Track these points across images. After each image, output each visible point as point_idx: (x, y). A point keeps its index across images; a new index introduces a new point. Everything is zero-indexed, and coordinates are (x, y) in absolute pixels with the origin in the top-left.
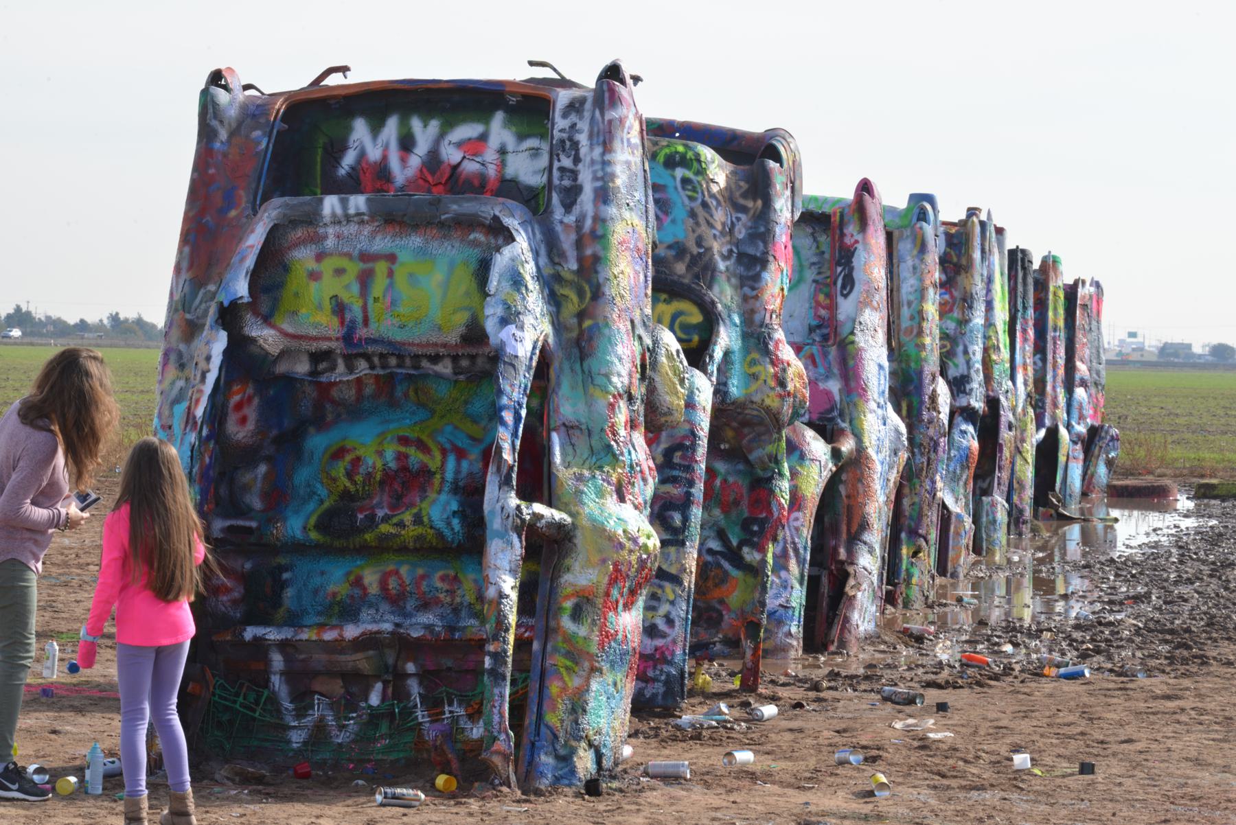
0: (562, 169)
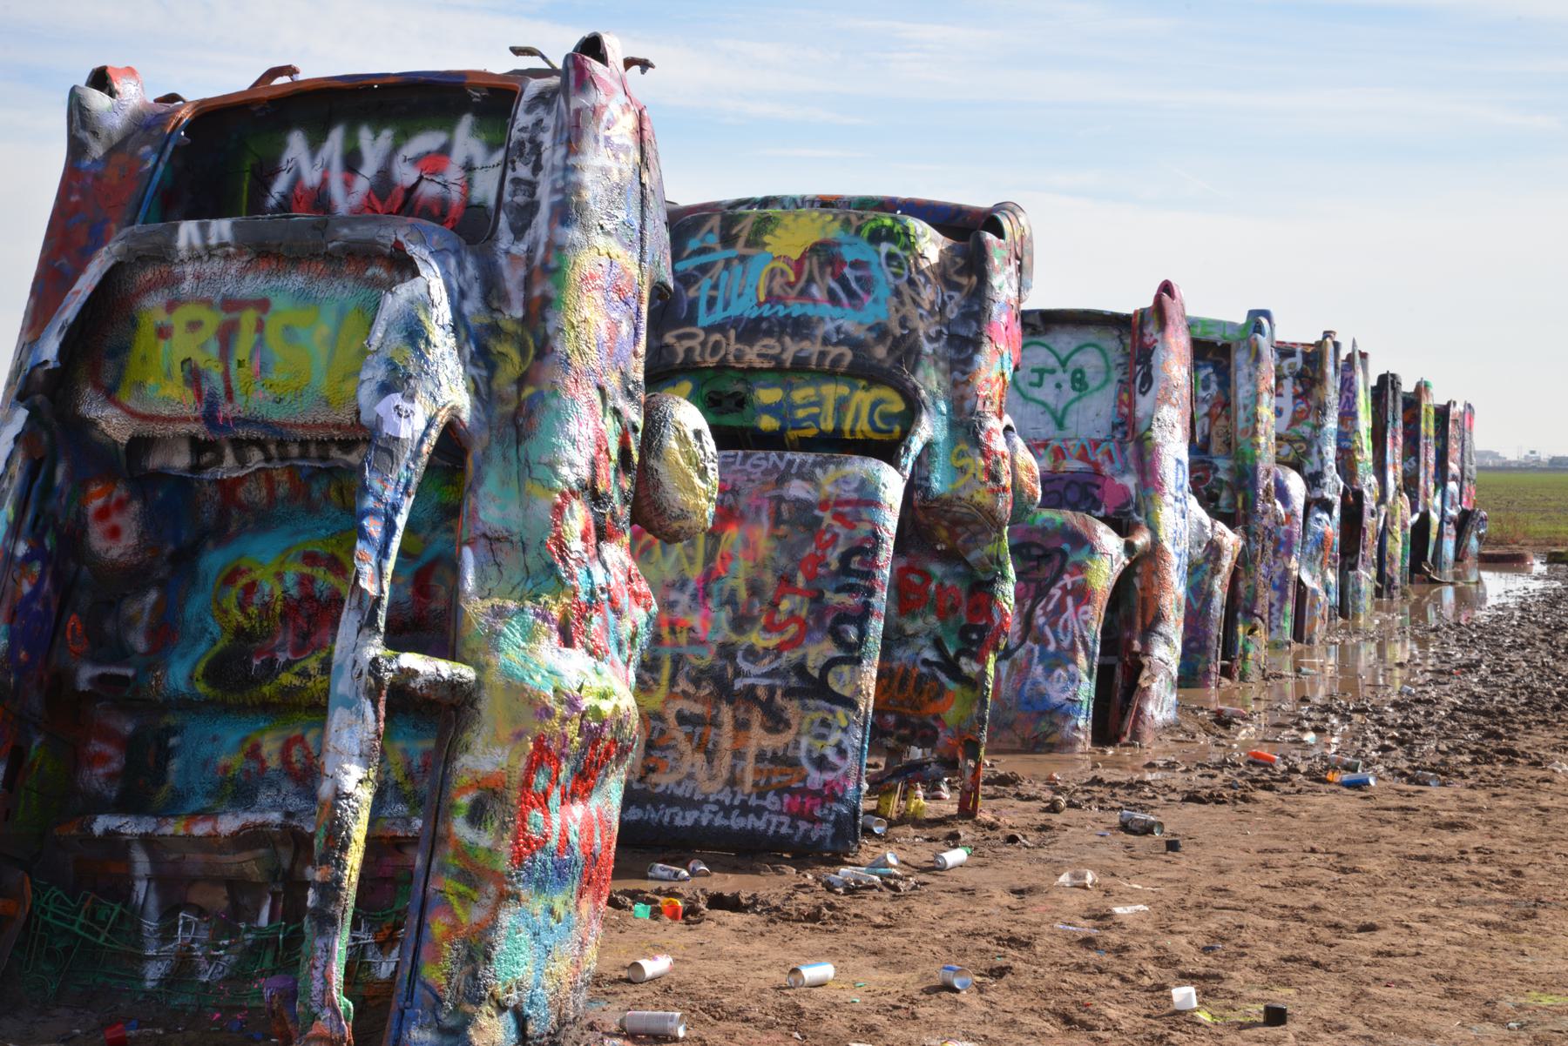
0: (517, 181)
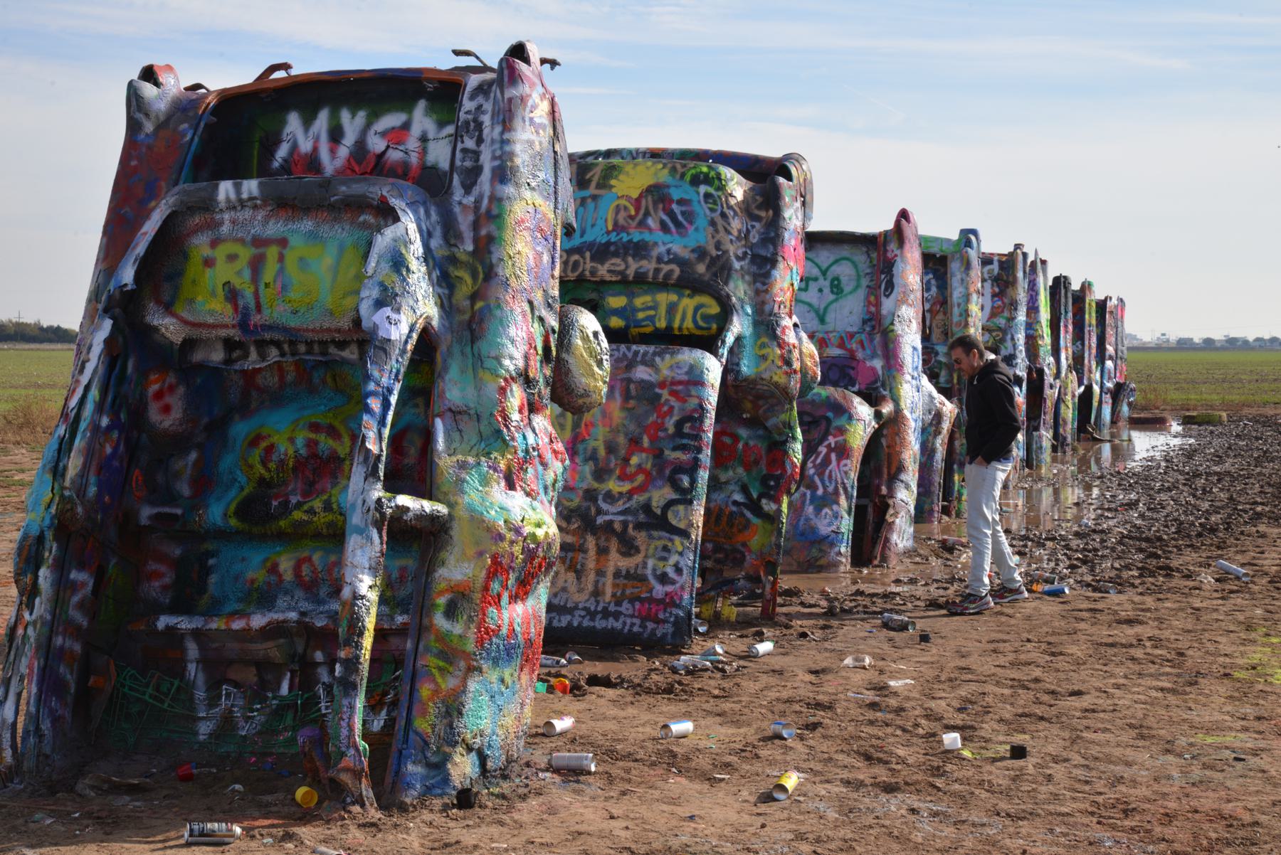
0: (465, 151)
